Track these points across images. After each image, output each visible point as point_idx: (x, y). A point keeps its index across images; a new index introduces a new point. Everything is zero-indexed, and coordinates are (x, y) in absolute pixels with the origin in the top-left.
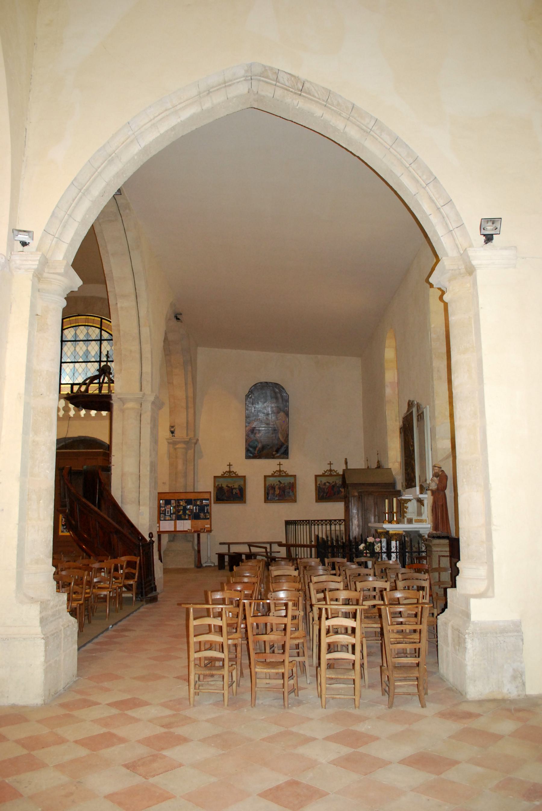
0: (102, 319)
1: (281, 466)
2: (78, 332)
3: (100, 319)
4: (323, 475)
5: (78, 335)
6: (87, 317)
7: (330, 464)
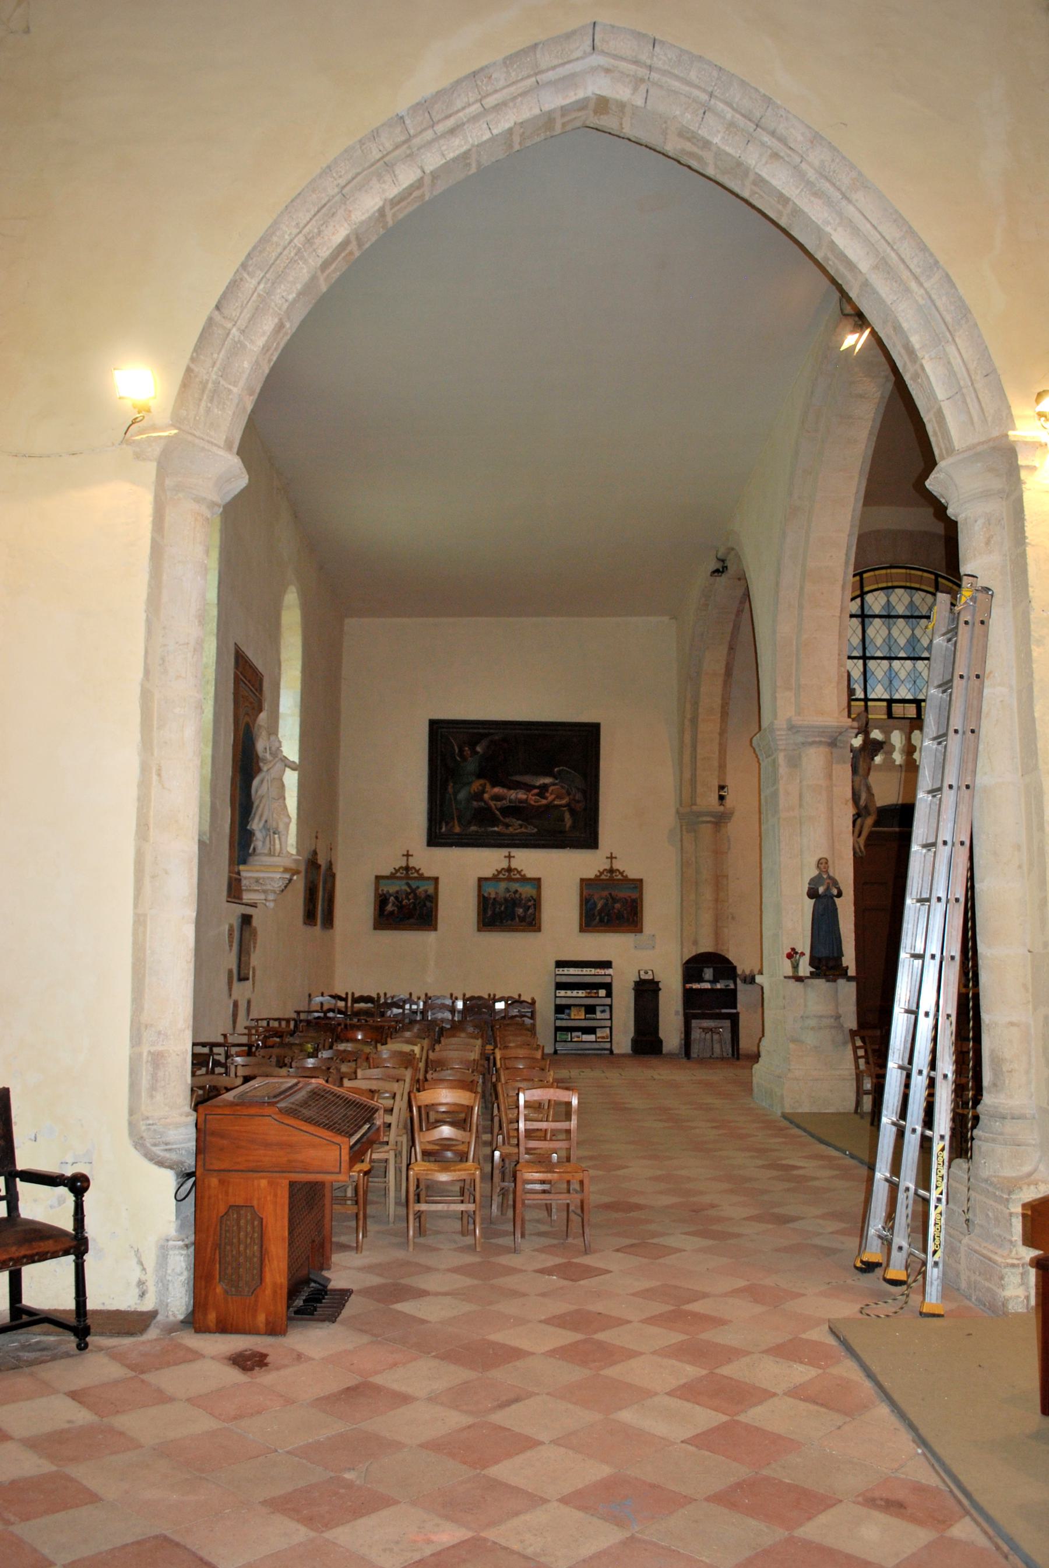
0: (937, 576)
1: (614, 860)
2: (894, 599)
3: (933, 577)
5: (894, 604)
6: (908, 571)
7: (408, 855)
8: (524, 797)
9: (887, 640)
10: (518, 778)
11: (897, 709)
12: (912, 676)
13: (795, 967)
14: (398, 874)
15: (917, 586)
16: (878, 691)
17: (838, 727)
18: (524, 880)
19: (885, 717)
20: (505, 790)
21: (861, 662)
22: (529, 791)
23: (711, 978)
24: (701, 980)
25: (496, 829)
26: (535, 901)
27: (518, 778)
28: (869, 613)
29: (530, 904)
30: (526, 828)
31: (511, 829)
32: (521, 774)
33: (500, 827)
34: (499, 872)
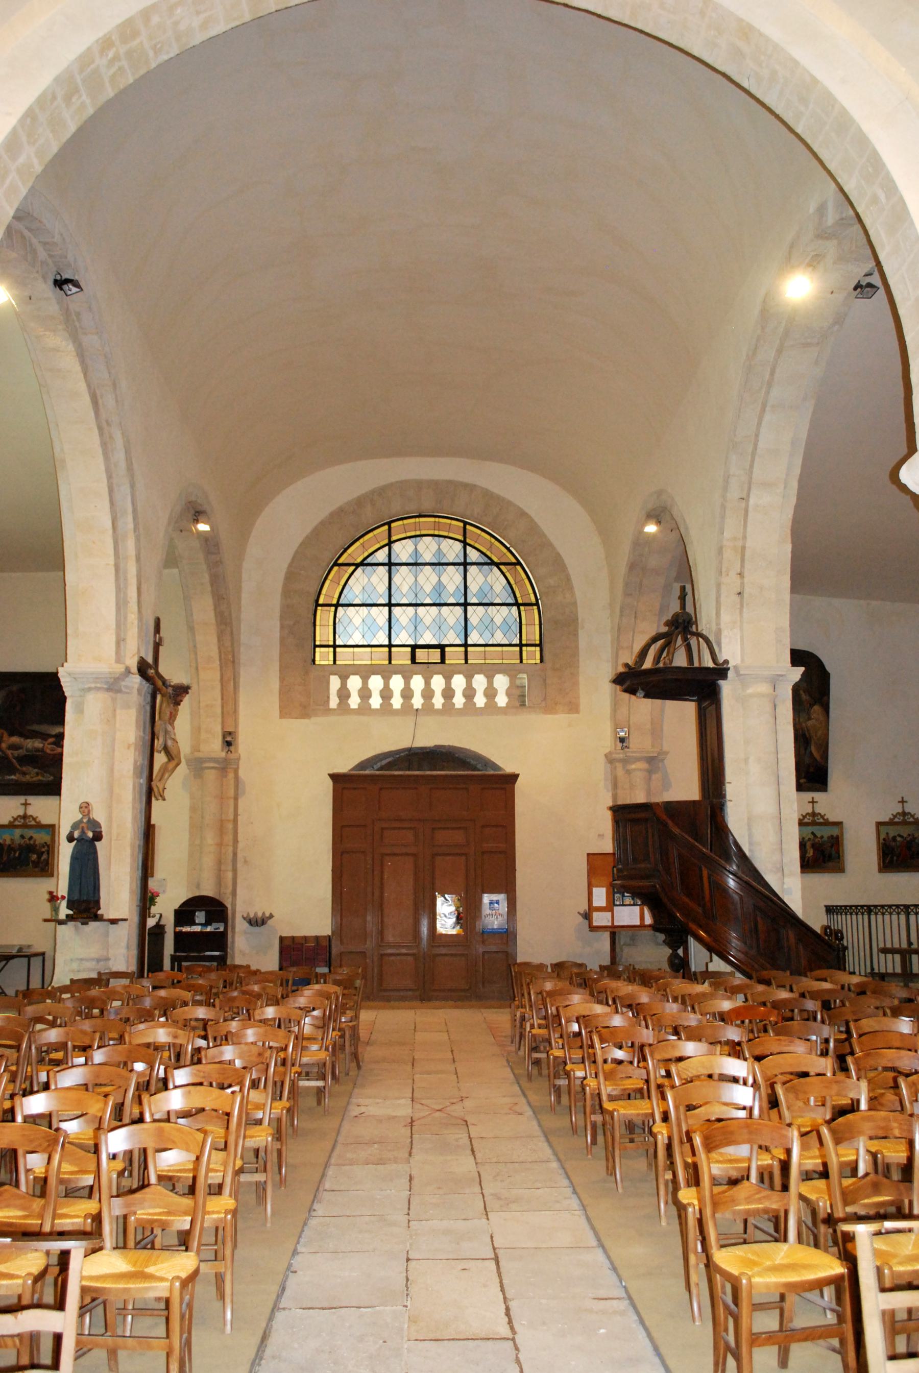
0: (465, 523)
1: (28, 806)
3: (461, 524)
4: (891, 823)
6: (437, 520)
8: (41, 745)
9: (413, 588)
10: (36, 727)
11: (421, 655)
12: (438, 621)
13: (56, 910)
14: (896, 820)
15: (445, 534)
16: (402, 637)
17: (110, 673)
18: (40, 826)
19: (409, 662)
20: (22, 740)
21: (387, 608)
22: (46, 740)
23: (204, 922)
24: (193, 923)
25: (13, 777)
26: (48, 846)
27: (36, 727)
28: (395, 562)
29: (43, 850)
30: (43, 776)
31: (28, 777)
32: (40, 723)
33: (17, 775)
34: (15, 819)
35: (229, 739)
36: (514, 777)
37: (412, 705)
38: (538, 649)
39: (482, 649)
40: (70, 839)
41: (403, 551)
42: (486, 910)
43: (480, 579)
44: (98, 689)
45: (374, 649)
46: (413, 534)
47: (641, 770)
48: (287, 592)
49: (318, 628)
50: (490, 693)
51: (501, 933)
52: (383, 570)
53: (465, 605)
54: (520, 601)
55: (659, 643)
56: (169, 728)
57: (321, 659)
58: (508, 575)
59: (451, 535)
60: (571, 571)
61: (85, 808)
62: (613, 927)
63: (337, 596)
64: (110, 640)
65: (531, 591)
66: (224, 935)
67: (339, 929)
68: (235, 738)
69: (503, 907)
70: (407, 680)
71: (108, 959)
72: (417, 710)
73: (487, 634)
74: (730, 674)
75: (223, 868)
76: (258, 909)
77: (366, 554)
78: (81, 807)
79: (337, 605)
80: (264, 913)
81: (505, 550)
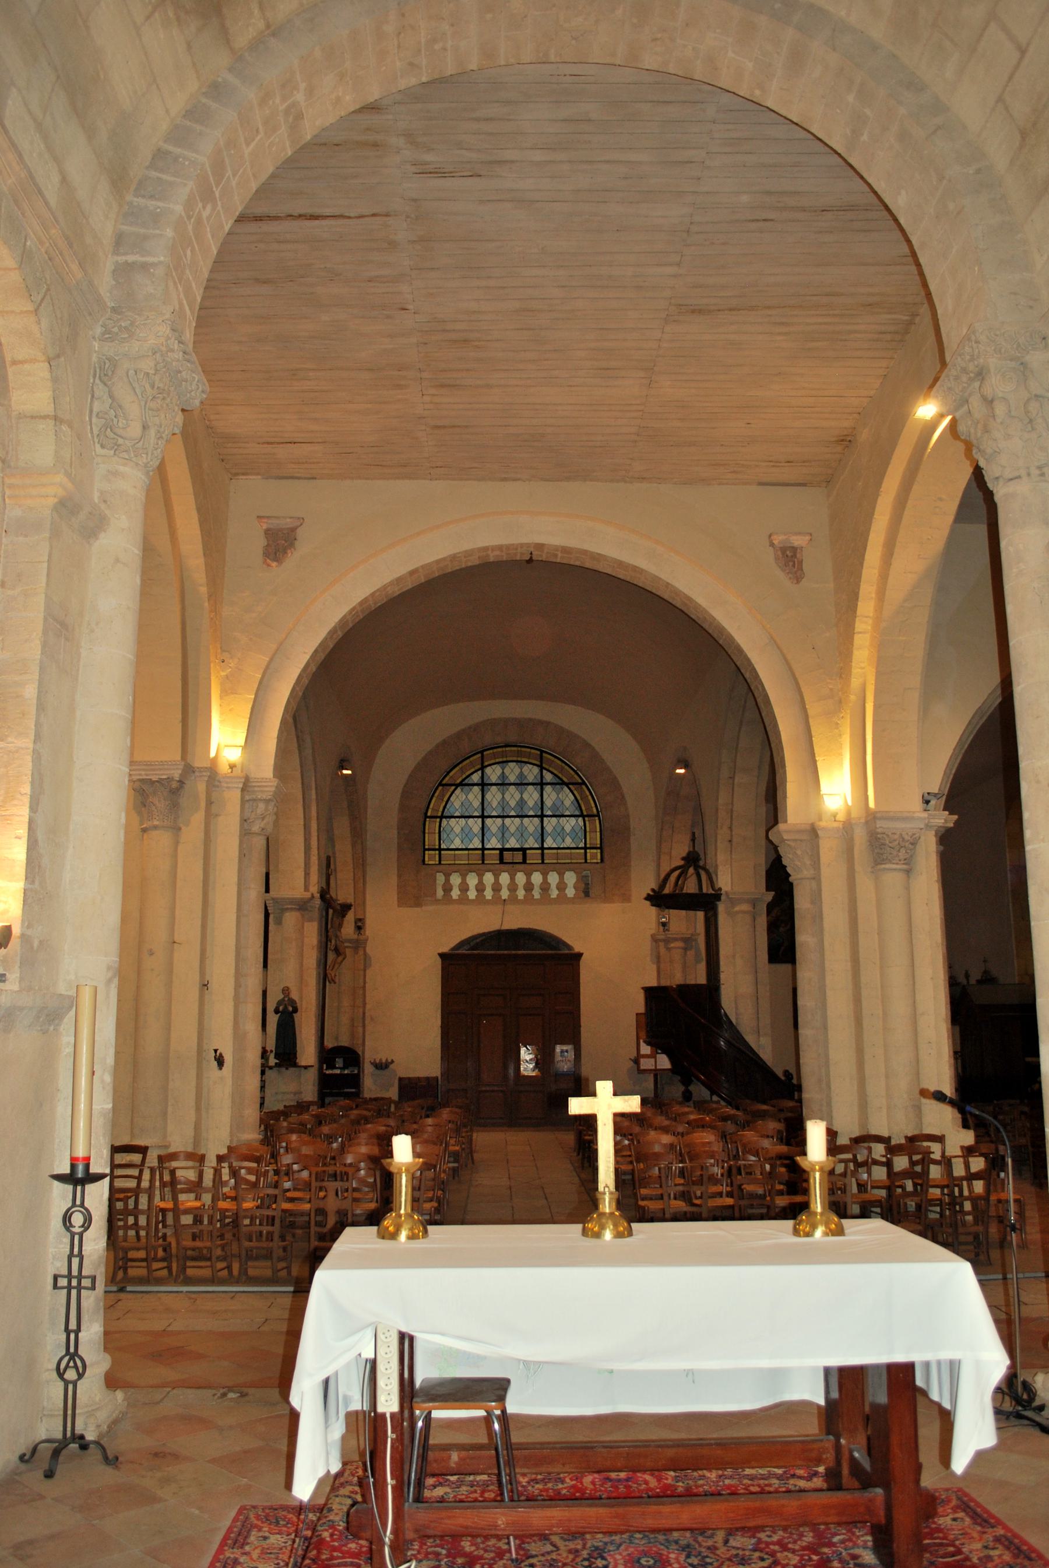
0: (542, 752)
3: (539, 753)
16: (493, 843)
21: (480, 820)
35: (359, 924)
36: (580, 955)
37: (501, 896)
38: (599, 851)
39: (555, 851)
40: (277, 1011)
41: (493, 773)
42: (558, 1057)
43: (554, 796)
44: (292, 909)
45: (471, 852)
46: (501, 760)
47: (678, 948)
48: (403, 808)
49: (427, 835)
50: (562, 887)
51: (569, 1075)
52: (476, 789)
53: (542, 816)
54: (585, 813)
55: (677, 873)
56: (338, 933)
57: (429, 860)
58: (575, 792)
59: (531, 761)
60: (625, 790)
61: (286, 991)
62: (656, 1070)
63: (441, 809)
64: (300, 874)
65: (593, 805)
66: (358, 1075)
67: (446, 1073)
68: (364, 924)
69: (571, 1055)
70: (497, 877)
71: (301, 1093)
72: (505, 900)
73: (559, 839)
74: (723, 898)
75: (355, 1025)
76: (382, 1056)
77: (464, 776)
78: (283, 990)
79: (442, 817)
80: (387, 1060)
81: (573, 773)
